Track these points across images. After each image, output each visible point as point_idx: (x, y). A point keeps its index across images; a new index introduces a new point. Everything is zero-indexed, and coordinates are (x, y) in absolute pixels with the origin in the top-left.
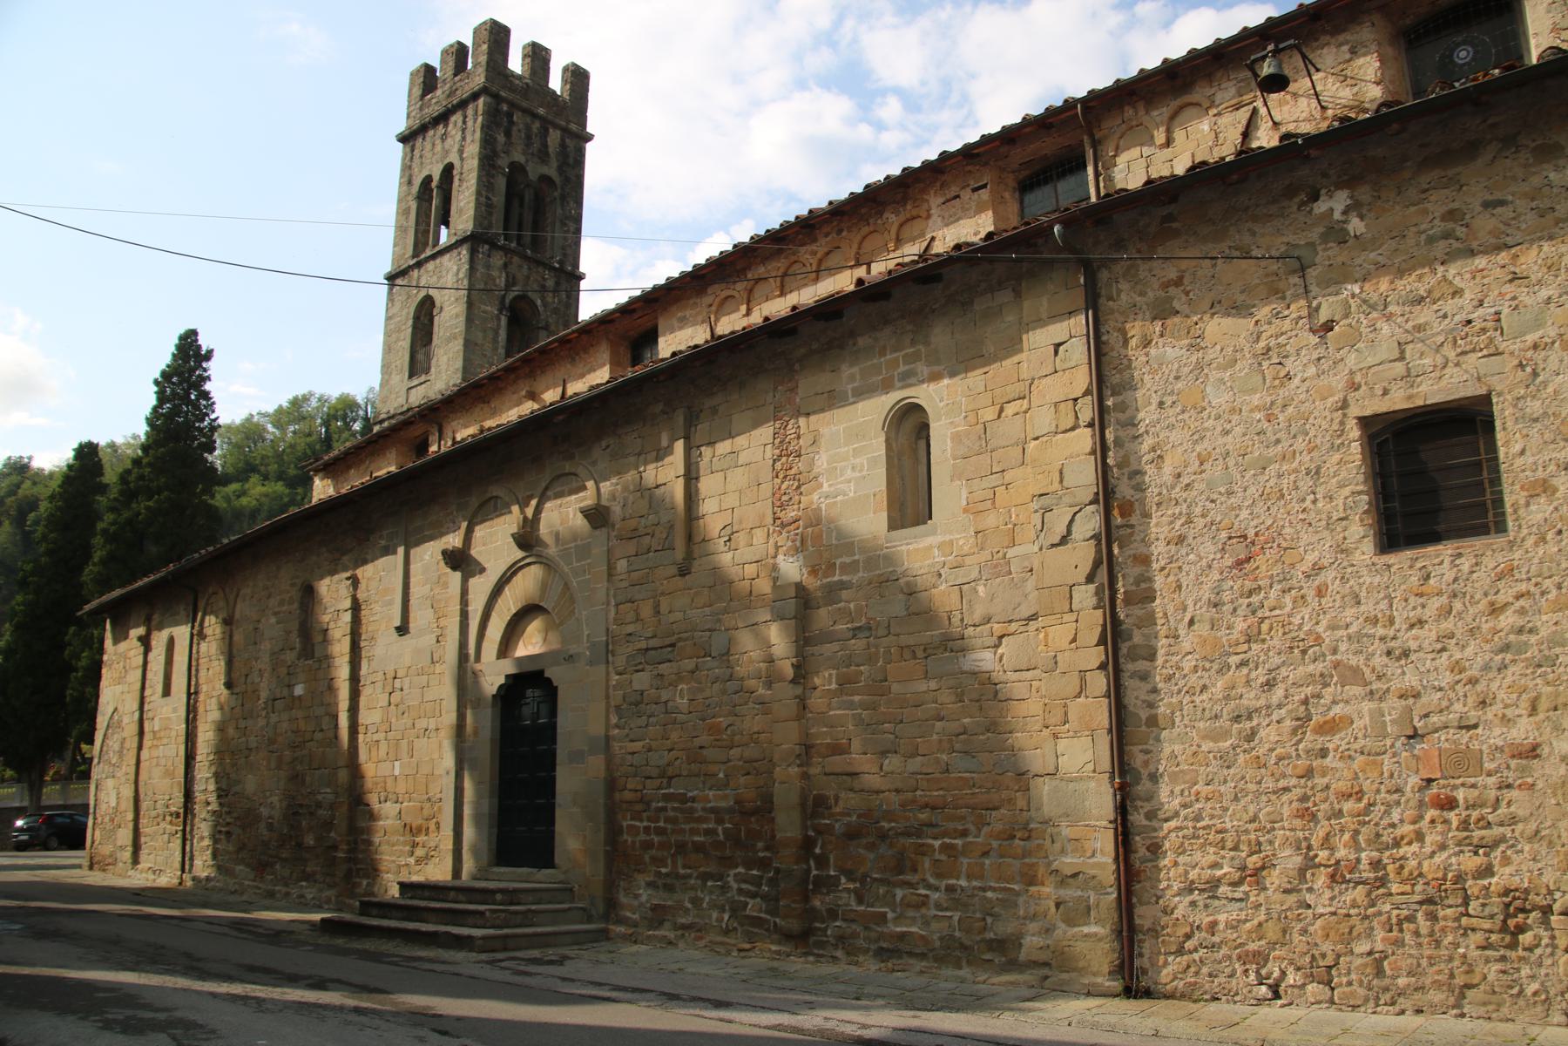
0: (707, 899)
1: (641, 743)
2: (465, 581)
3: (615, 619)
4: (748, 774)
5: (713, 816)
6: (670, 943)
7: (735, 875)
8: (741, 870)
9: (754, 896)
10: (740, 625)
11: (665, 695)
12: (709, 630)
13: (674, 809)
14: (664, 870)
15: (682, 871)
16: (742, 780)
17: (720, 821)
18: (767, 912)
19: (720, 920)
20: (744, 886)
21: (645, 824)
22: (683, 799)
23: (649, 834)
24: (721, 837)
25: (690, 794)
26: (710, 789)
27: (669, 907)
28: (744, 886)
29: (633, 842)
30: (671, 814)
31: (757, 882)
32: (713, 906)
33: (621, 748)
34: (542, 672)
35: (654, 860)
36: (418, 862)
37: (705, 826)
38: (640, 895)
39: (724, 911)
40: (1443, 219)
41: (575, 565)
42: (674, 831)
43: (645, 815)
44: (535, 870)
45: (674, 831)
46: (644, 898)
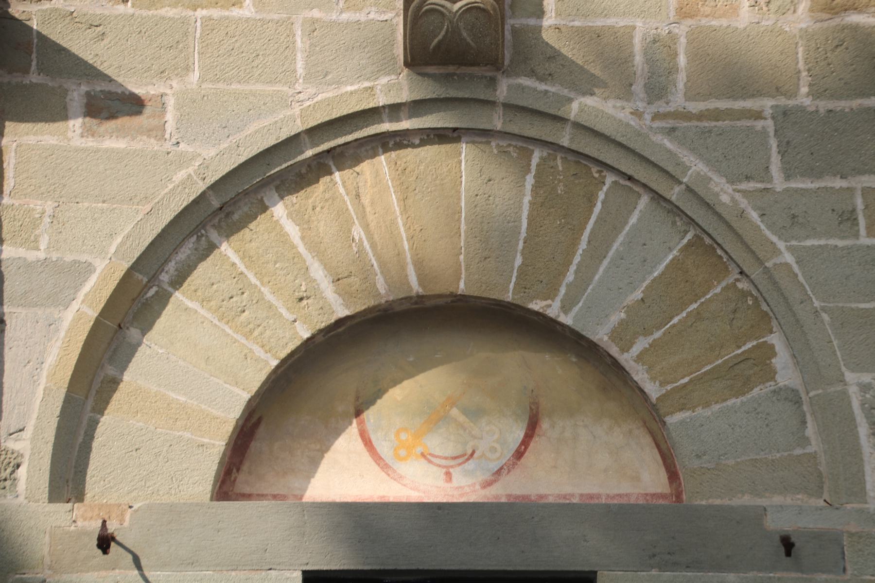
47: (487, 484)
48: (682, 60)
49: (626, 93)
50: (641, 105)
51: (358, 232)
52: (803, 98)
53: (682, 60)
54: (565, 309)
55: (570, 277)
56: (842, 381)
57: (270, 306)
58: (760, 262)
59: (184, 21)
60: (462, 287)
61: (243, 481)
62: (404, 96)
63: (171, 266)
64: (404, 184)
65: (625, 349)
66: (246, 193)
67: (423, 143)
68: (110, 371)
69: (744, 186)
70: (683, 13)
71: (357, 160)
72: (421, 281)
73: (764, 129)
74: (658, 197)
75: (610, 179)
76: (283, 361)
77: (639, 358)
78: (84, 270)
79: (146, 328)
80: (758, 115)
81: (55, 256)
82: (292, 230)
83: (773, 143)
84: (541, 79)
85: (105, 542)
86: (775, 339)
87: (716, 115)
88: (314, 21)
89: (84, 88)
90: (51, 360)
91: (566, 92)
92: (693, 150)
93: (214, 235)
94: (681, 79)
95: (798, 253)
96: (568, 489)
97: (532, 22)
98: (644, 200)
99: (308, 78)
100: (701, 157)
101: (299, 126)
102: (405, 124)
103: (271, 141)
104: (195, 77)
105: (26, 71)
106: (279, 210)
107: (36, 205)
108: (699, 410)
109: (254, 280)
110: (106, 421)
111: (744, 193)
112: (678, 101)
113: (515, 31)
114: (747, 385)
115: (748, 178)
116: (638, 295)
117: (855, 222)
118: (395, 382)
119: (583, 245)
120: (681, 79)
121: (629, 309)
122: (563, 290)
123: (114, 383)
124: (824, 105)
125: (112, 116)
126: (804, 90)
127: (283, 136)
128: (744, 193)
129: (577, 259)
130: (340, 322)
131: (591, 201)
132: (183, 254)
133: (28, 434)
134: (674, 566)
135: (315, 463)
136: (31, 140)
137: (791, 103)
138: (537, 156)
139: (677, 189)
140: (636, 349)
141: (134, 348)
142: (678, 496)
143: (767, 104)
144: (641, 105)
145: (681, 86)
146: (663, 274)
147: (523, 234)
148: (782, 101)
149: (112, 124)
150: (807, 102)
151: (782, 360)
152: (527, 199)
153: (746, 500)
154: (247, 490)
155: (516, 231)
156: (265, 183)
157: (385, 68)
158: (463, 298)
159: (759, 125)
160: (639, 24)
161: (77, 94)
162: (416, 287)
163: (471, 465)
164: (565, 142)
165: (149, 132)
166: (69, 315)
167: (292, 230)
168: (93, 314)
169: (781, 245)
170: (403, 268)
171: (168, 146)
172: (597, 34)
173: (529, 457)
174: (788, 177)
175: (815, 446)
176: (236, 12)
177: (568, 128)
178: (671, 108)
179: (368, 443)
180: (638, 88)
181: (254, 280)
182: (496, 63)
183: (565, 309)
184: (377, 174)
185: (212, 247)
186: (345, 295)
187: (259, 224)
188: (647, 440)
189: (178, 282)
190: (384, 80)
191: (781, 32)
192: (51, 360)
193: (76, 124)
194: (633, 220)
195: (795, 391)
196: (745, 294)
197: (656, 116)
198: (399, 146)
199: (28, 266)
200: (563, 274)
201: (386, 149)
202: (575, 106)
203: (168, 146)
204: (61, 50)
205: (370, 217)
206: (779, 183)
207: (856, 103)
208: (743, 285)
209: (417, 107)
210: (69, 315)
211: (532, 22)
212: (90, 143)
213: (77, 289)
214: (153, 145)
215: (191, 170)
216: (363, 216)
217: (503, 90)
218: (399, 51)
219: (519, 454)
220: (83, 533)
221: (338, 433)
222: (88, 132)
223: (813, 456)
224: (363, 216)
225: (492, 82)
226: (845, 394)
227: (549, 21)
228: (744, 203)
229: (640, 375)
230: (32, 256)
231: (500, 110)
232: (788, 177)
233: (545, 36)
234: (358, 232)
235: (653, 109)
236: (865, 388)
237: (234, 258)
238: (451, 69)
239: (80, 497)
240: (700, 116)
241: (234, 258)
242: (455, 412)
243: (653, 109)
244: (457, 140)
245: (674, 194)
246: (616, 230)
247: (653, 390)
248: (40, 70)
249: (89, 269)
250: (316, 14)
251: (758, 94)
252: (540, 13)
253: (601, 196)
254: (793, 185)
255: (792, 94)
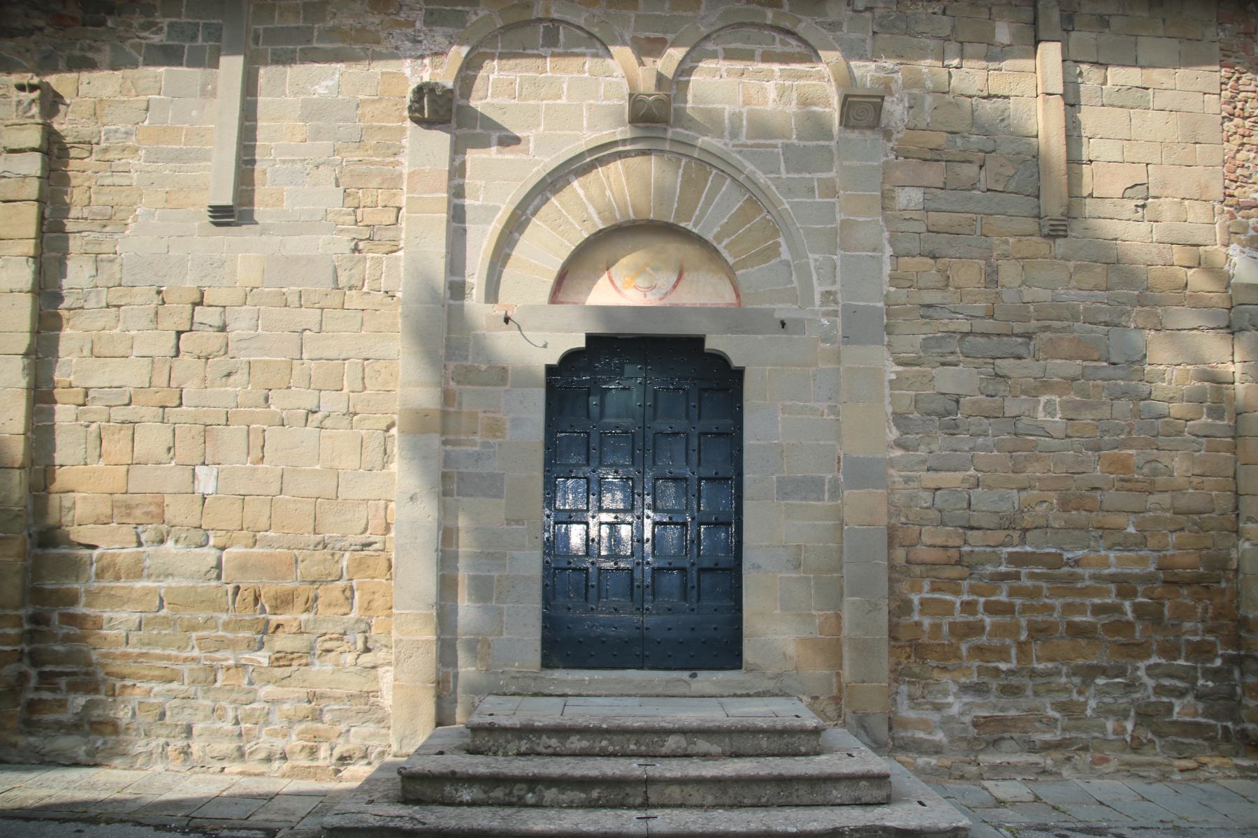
0: (1092, 703)
1: (960, 475)
2: (458, 149)
3: (892, 278)
4: (1182, 529)
5: (1113, 587)
6: (1044, 772)
7: (1149, 668)
8: (1154, 660)
9: (1181, 694)
10: (119, 276)
11: (1012, 408)
12: (1106, 324)
13: (1032, 576)
14: (1003, 666)
15: (1040, 666)
16: (1173, 538)
17: (1124, 593)
18: (1205, 715)
19: (1120, 731)
20: (1167, 682)
21: (966, 597)
22: (1055, 562)
23: (974, 613)
24: (1130, 616)
25: (1067, 555)
26: (1110, 549)
27: (1013, 718)
28: (1167, 682)
29: (936, 628)
30: (1026, 582)
31: (1188, 675)
32: (1103, 711)
33: (907, 480)
34: (700, 340)
35: (979, 651)
36: (281, 659)
37: (1097, 601)
38: (949, 705)
39: (1126, 717)
40: (257, 44)
41: (784, 175)
42: (1025, 609)
43: (965, 584)
44: (685, 675)
45: (1025, 609)
46: (955, 710)
47: (661, 299)
48: (745, 123)
49: (721, 136)
50: (727, 141)
51: (608, 193)
52: (794, 140)
53: (745, 123)
54: (695, 226)
55: (697, 212)
56: (807, 258)
57: (572, 224)
58: (776, 207)
59: (538, 106)
60: (652, 216)
61: (561, 297)
62: (628, 136)
63: (531, 207)
64: (144, 106)
65: (719, 243)
66: (562, 177)
67: (636, 156)
68: (507, 250)
69: (769, 176)
70: (746, 103)
71: (608, 162)
72: (635, 214)
73: (778, 153)
74: (734, 179)
75: (714, 171)
76: (577, 247)
77: (725, 247)
78: (497, 209)
79: (521, 233)
80: (775, 146)
81: (485, 203)
82: (581, 192)
83: (782, 158)
84: (686, 129)
85: (507, 320)
86: (781, 240)
87: (758, 146)
88: (591, 105)
89: (498, 134)
90: (484, 246)
91: (696, 135)
92: (749, 160)
93: (549, 194)
94: (744, 130)
95: (793, 206)
96: (695, 301)
97: (682, 105)
98: (729, 181)
99: (588, 128)
100: (752, 163)
101: (584, 148)
102: (628, 148)
103: (572, 155)
104: (542, 128)
105: (475, 128)
106: (576, 184)
107: (478, 182)
108: (750, 269)
109: (565, 213)
110: (506, 271)
111: (770, 178)
112: (743, 139)
113: (675, 109)
114: (769, 259)
115: (771, 172)
116: (725, 220)
117: (814, 192)
118: (623, 257)
119: (703, 199)
120: (744, 130)
121: (721, 226)
122: (694, 218)
123: (508, 256)
124: (802, 143)
125: (508, 146)
126: (794, 137)
127: (578, 152)
128: (770, 178)
129: (700, 205)
130: (600, 231)
131: (706, 181)
132: (536, 202)
133: (476, 276)
134: (738, 332)
135: (590, 289)
136: (477, 156)
137: (789, 142)
138: (684, 161)
139: (742, 176)
140: (724, 243)
141: (516, 241)
142: (740, 305)
143: (779, 142)
144: (727, 141)
145: (744, 133)
146: (736, 212)
147: (678, 194)
148: (785, 141)
149: (508, 149)
150: (796, 141)
151: (784, 249)
152: (679, 179)
153: (767, 306)
154: (562, 300)
155: (675, 193)
156: (570, 173)
157: (621, 124)
158: (652, 221)
159: (776, 150)
160: (727, 107)
161: (495, 136)
162: (632, 216)
163: (654, 291)
164: (696, 155)
165: (522, 152)
166: (491, 228)
167: (581, 192)
168: (500, 227)
169: (784, 201)
170: (627, 207)
171: (530, 157)
172: (710, 111)
173: (679, 288)
174: (787, 173)
175: (796, 284)
176: (559, 102)
177: (697, 150)
178: (740, 142)
179: (612, 281)
180: (726, 133)
181: (565, 213)
182: (667, 122)
183: (695, 226)
184: (616, 168)
185: (548, 199)
186: (603, 219)
187: (567, 190)
188: (727, 281)
189: (534, 214)
190: (620, 129)
191: (785, 112)
192: (484, 246)
193: (494, 149)
194: (724, 189)
195: (788, 262)
196: (769, 221)
197: (734, 146)
198: (626, 157)
199: (475, 208)
200: (694, 211)
201: (620, 158)
202: (700, 140)
203: (530, 157)
204: (489, 119)
205: (613, 187)
206: (784, 175)
207: (815, 143)
208: (769, 217)
209: (634, 140)
210: (491, 228)
211: (682, 105)
212: (500, 156)
213: (494, 217)
214: (525, 157)
215: (539, 167)
216: (610, 186)
217: (670, 133)
218: (626, 117)
219: (675, 287)
220: (498, 316)
221: (599, 277)
222: (499, 152)
223: (795, 288)
224: (610, 186)
225: (665, 130)
226: (808, 263)
227: (689, 105)
228: (769, 183)
229: (725, 254)
230: (477, 203)
231: (668, 142)
232: (787, 173)
233: (688, 111)
234: (608, 193)
235: (732, 143)
236: (816, 260)
237: (557, 203)
238: (648, 124)
239: (496, 302)
240: (752, 146)
241: (557, 203)
242: (648, 269)
243: (732, 143)
244: (650, 154)
245: (741, 178)
246: (717, 193)
247: (731, 261)
248: (481, 127)
249: (499, 208)
250: (592, 101)
251: (775, 137)
252: (686, 102)
253: (711, 178)
254: (790, 176)
255: (789, 138)
